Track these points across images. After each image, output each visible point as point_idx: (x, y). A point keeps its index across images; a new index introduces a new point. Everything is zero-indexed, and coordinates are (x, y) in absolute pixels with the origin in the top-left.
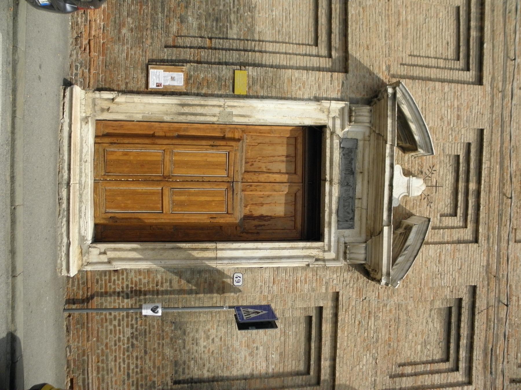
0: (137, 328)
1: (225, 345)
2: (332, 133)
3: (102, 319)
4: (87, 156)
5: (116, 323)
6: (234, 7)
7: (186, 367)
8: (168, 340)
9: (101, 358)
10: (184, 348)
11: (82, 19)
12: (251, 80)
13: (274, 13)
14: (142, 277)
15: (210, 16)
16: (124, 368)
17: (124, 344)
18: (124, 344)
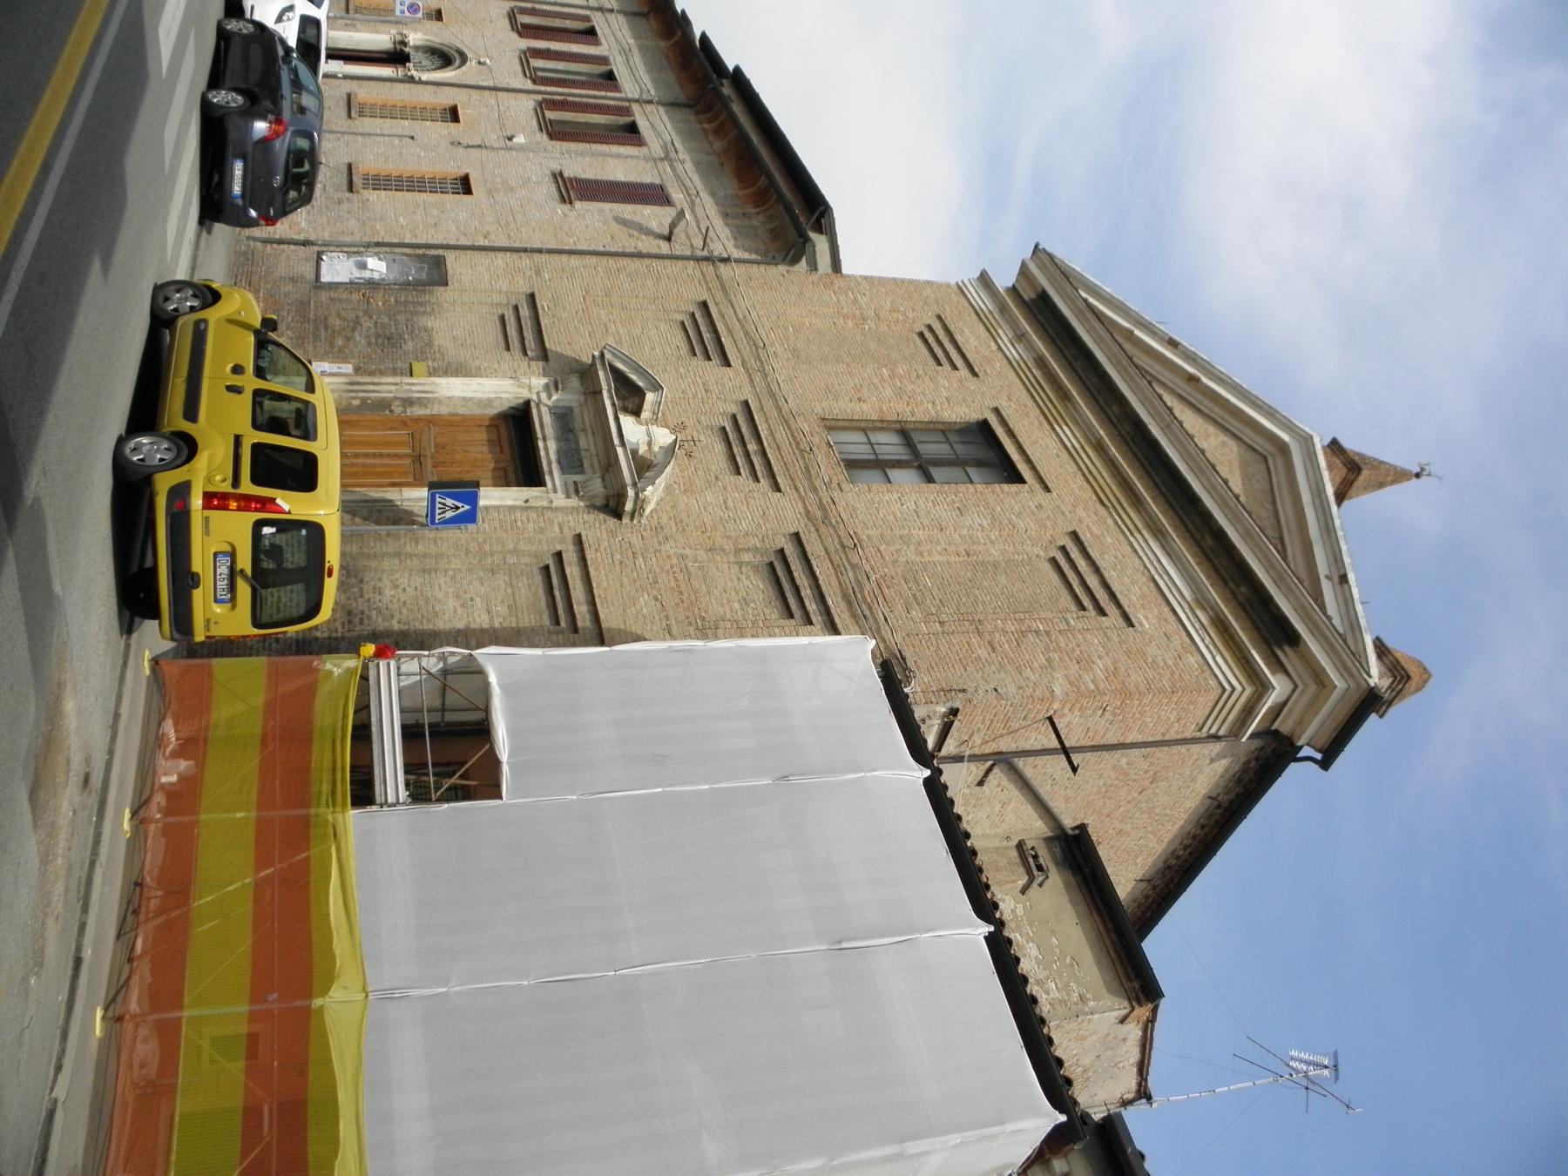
1: (422, 595)
2: (538, 405)
7: (365, 616)
10: (362, 596)
16: (272, 602)
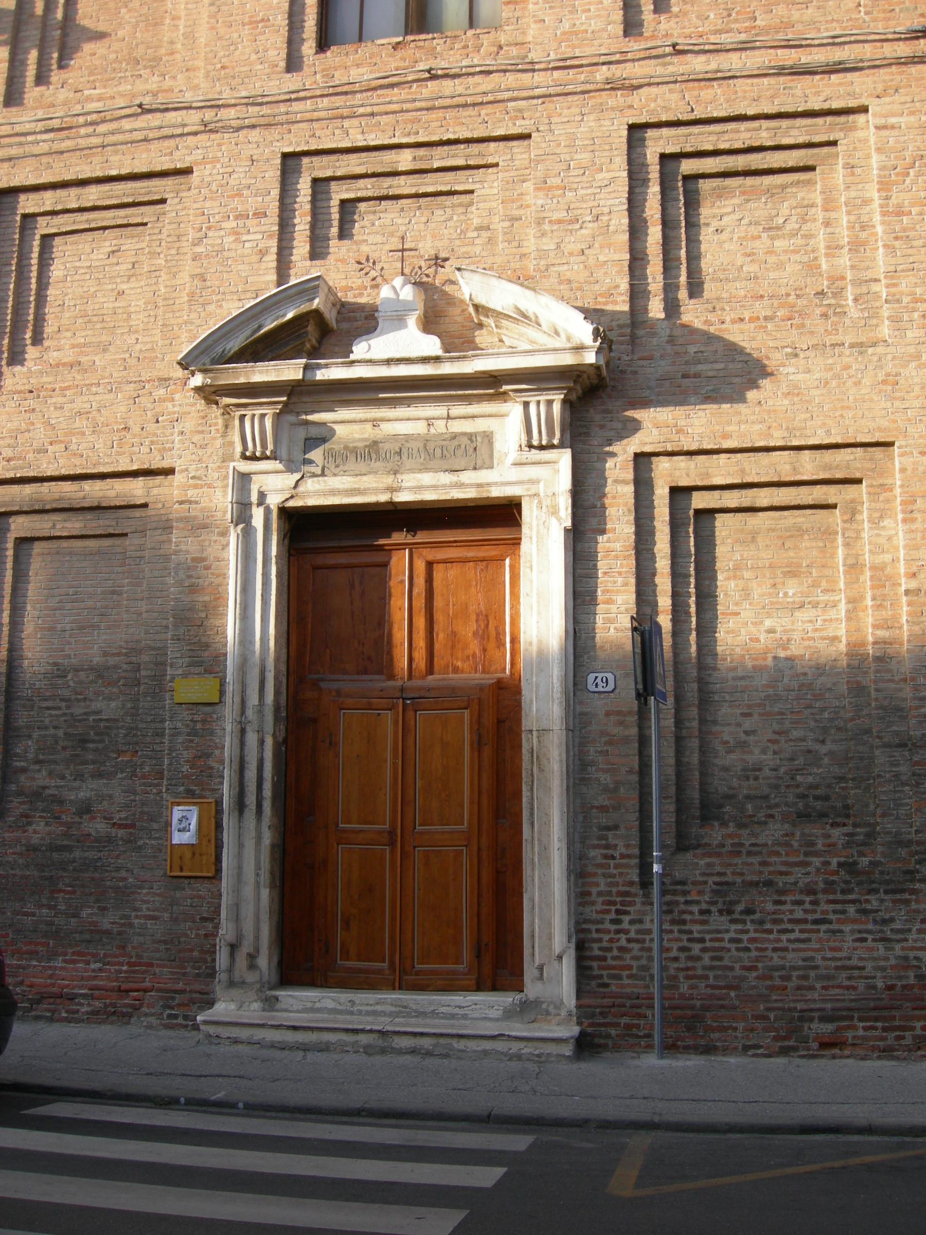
0: (707, 903)
1: (759, 705)
3: (688, 977)
4: (342, 1001)
5: (696, 948)
6: (59, 708)
8: (745, 832)
9: (778, 982)
10: (766, 797)
11: (82, 1005)
12: (192, 669)
13: (68, 627)
14: (594, 890)
15: (78, 755)
16: (801, 931)
17: (747, 932)
18: (747, 932)
